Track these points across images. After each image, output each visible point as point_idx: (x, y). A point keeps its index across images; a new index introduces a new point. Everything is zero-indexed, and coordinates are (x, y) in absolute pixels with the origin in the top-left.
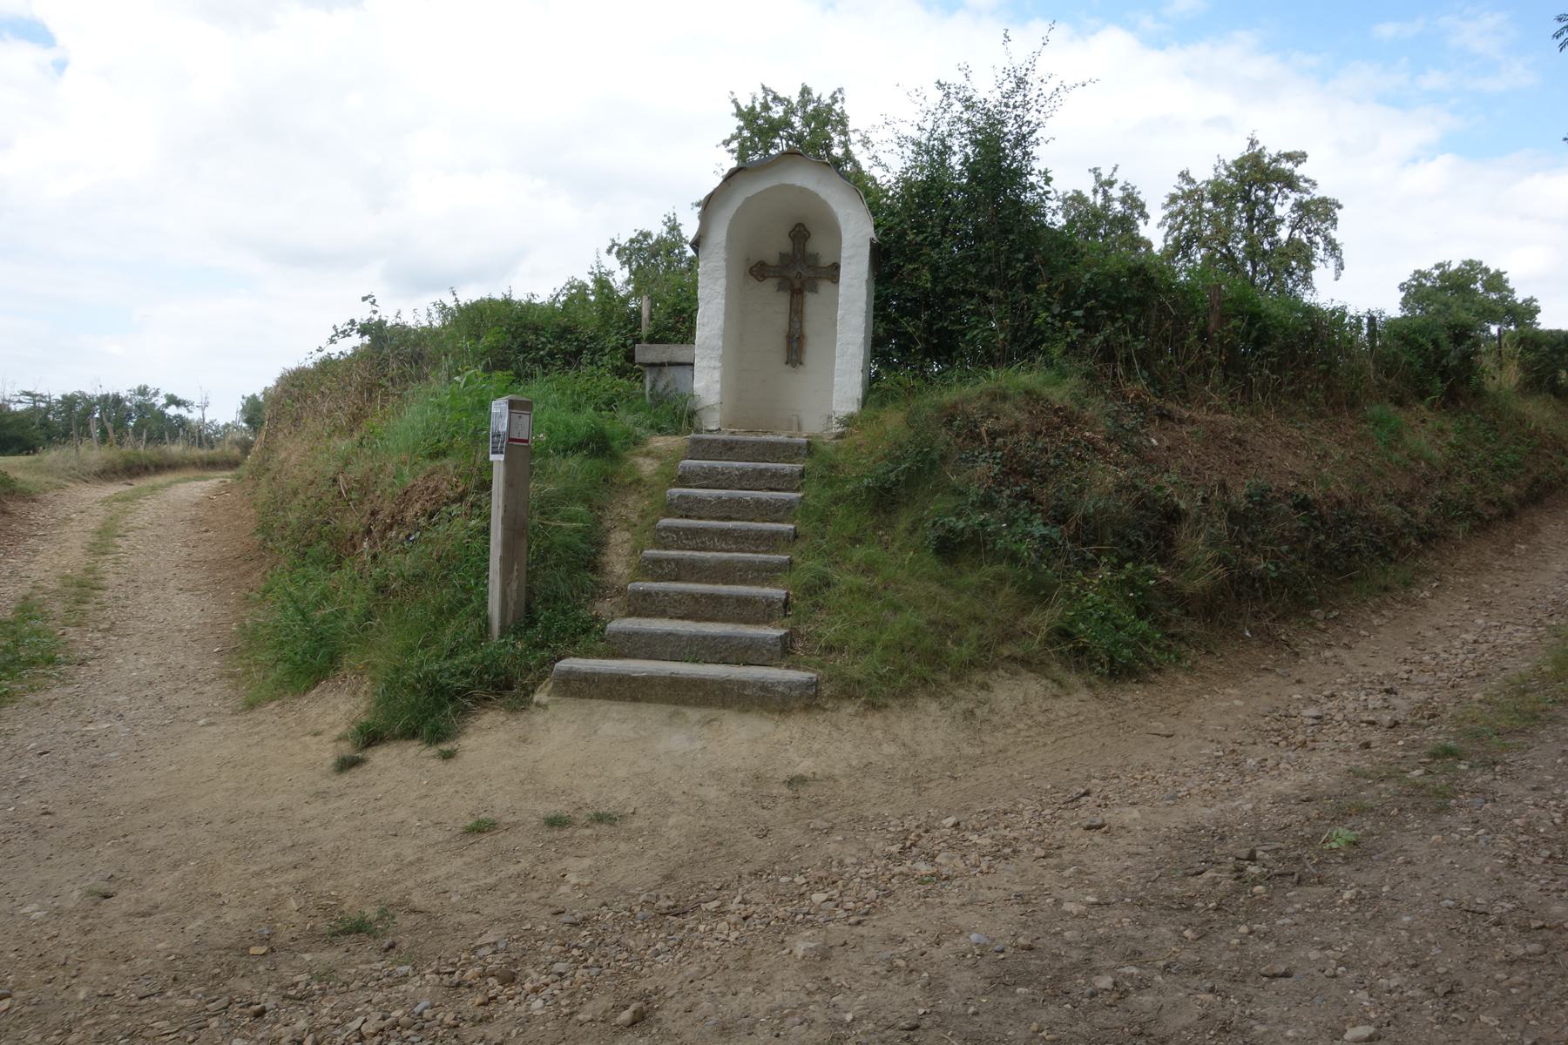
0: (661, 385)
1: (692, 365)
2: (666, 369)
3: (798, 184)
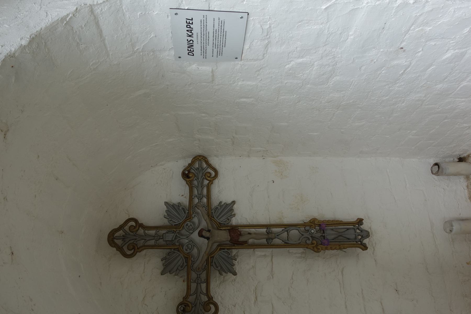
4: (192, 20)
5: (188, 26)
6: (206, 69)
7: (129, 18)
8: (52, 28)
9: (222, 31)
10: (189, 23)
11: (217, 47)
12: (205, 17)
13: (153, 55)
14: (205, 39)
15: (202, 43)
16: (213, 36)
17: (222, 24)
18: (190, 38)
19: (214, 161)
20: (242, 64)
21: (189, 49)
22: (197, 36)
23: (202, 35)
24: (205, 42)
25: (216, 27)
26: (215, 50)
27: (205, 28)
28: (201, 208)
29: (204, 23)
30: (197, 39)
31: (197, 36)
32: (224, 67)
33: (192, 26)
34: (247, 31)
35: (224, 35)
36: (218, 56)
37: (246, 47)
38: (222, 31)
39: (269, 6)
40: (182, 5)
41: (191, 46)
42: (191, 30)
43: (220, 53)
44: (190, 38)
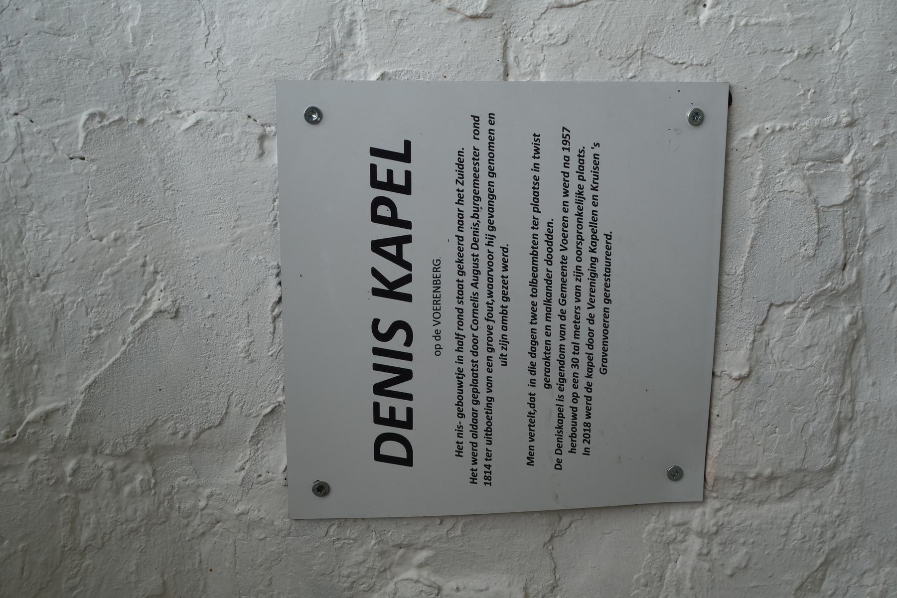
4: (405, 157)
5: (384, 211)
7: (20, 147)
9: (587, 232)
10: (389, 185)
11: (554, 378)
12: (484, 126)
13: (147, 488)
14: (483, 311)
15: (468, 344)
16: (534, 283)
18: (390, 311)
20: (710, 525)
21: (386, 403)
22: (437, 283)
23: (468, 279)
24: (482, 334)
25: (551, 209)
26: (546, 400)
27: (484, 215)
31: (437, 283)
33: (405, 205)
34: (730, 240)
35: (600, 268)
36: (566, 457)
37: (734, 363)
38: (587, 232)
39: (844, 26)
40: (350, 58)
41: (394, 379)
42: (400, 242)
44: (390, 311)
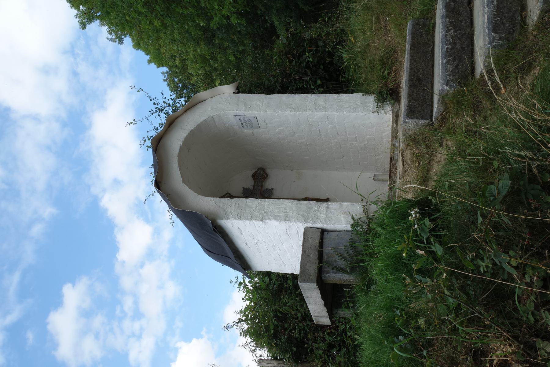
0: (340, 263)
1: (323, 231)
2: (325, 257)
3: (180, 143)
6: (250, 131)
8: (202, 123)
17: (249, 119)
19: (268, 171)
28: (389, 292)
29: (244, 119)
30: (118, 242)
32: (255, 131)
43: (252, 127)
